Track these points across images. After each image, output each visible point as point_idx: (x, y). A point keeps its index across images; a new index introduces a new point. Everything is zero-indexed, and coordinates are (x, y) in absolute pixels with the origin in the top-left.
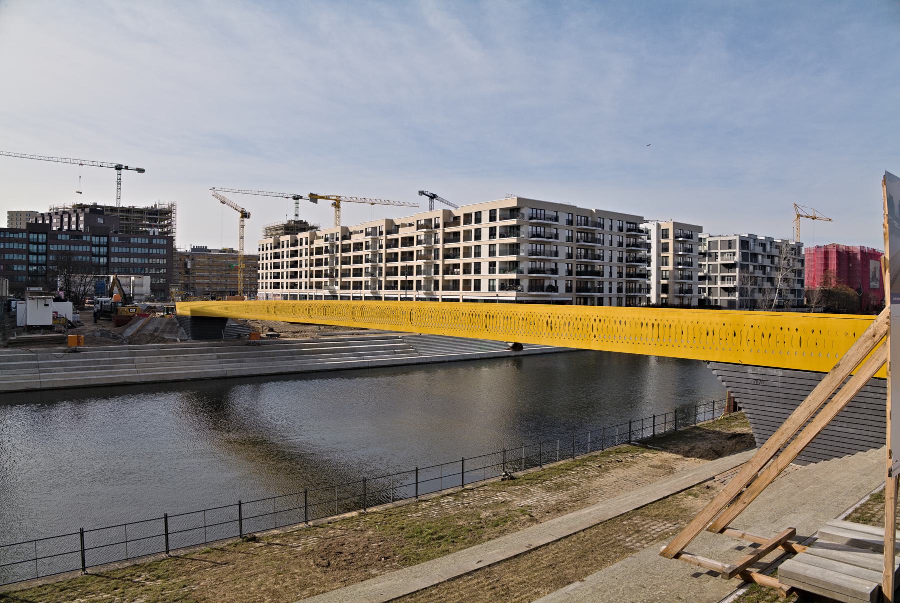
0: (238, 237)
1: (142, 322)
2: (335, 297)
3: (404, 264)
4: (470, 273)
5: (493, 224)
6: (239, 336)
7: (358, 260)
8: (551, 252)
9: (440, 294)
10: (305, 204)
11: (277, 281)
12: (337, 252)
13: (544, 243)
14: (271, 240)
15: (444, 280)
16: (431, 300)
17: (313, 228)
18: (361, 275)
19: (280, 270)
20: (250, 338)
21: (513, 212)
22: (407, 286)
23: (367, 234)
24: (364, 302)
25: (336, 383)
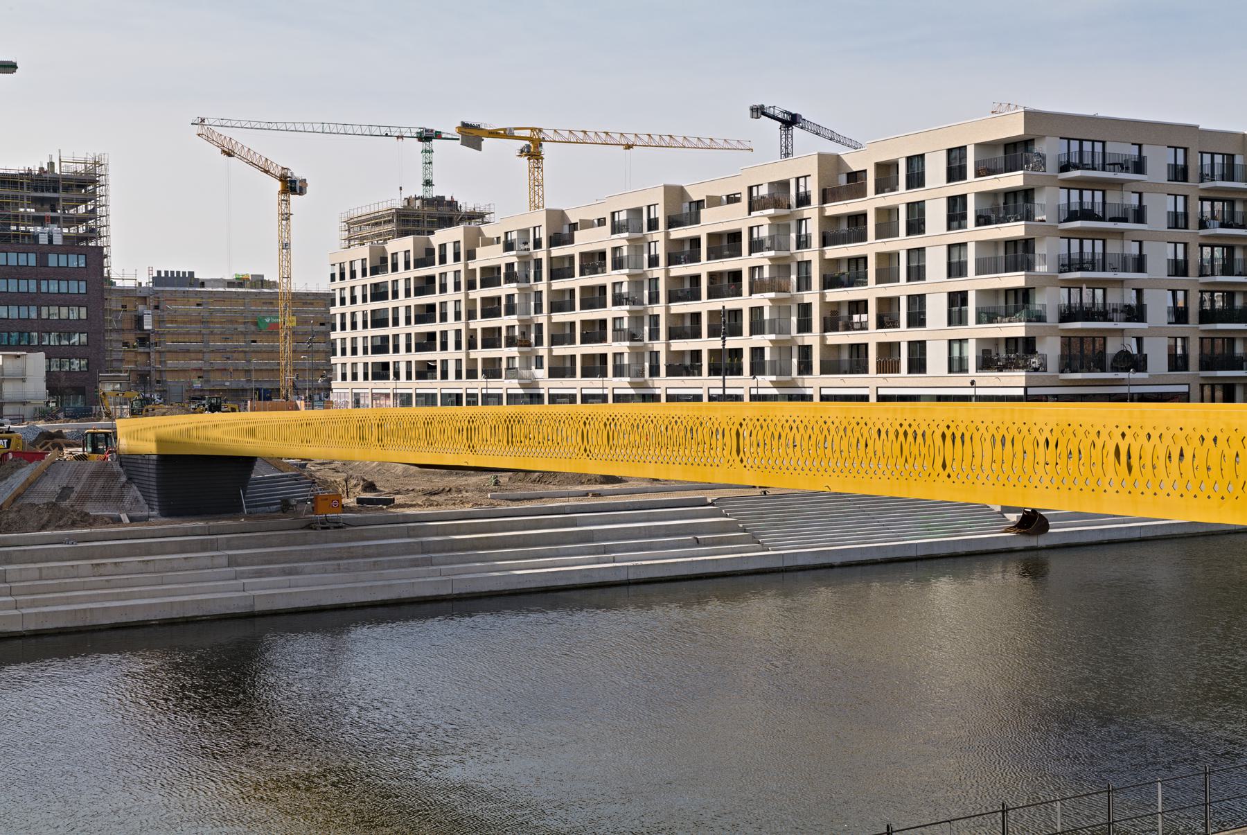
0: (276, 246)
1: (26, 472)
2: (536, 398)
3: (717, 304)
5: (957, 189)
6: (286, 506)
7: (594, 297)
8: (1124, 259)
10: (448, 151)
12: (538, 278)
13: (1104, 235)
14: (363, 252)
15: (825, 347)
17: (472, 216)
18: (603, 339)
19: (389, 331)
21: (1013, 152)
22: (726, 363)
23: (616, 228)
24: (611, 408)
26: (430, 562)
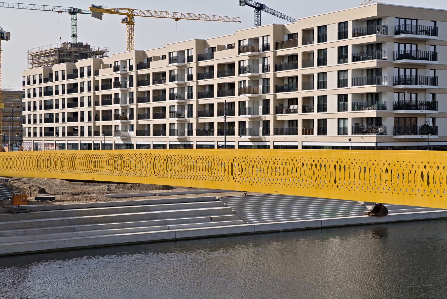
2: (130, 146)
3: (222, 100)
4: (311, 110)
5: (343, 43)
7: (160, 95)
8: (426, 78)
9: (271, 139)
11: (49, 125)
13: (416, 67)
14: (41, 70)
15: (276, 121)
16: (259, 147)
17: (99, 53)
18: (164, 117)
20: (12, 203)
21: (371, 25)
23: (171, 61)
24: (168, 152)
25: (127, 260)
26: (74, 230)
